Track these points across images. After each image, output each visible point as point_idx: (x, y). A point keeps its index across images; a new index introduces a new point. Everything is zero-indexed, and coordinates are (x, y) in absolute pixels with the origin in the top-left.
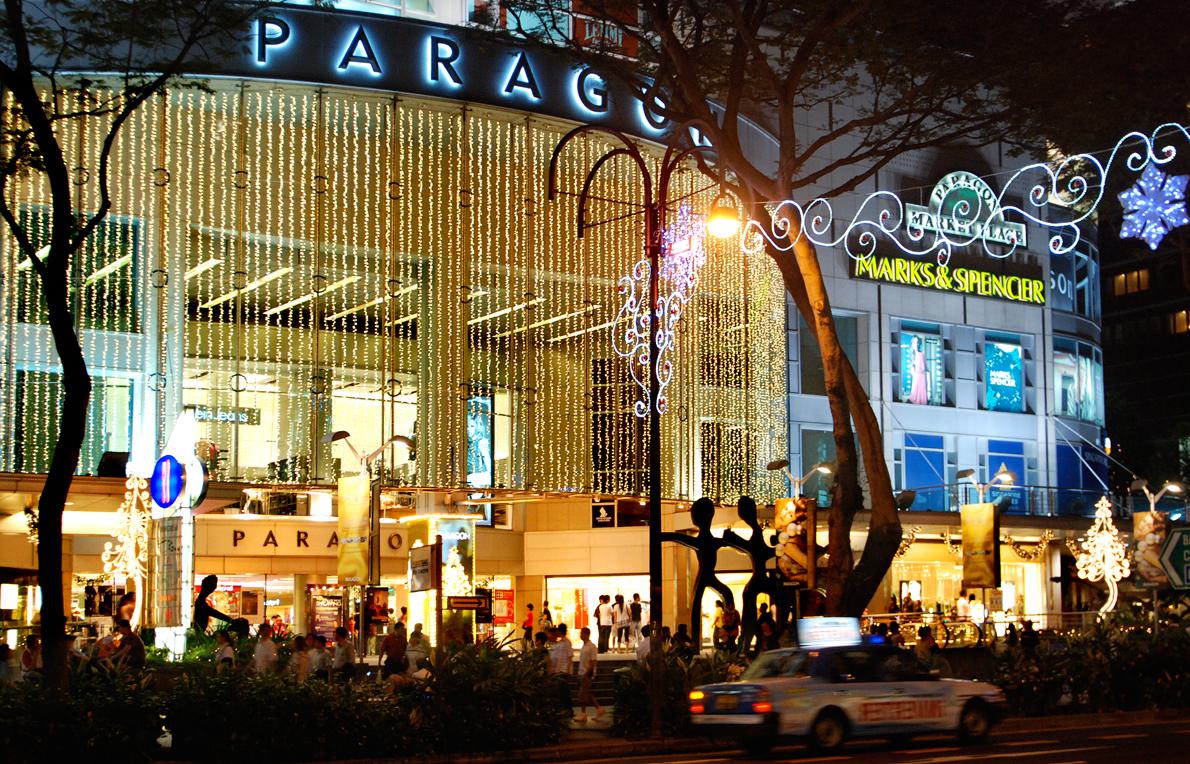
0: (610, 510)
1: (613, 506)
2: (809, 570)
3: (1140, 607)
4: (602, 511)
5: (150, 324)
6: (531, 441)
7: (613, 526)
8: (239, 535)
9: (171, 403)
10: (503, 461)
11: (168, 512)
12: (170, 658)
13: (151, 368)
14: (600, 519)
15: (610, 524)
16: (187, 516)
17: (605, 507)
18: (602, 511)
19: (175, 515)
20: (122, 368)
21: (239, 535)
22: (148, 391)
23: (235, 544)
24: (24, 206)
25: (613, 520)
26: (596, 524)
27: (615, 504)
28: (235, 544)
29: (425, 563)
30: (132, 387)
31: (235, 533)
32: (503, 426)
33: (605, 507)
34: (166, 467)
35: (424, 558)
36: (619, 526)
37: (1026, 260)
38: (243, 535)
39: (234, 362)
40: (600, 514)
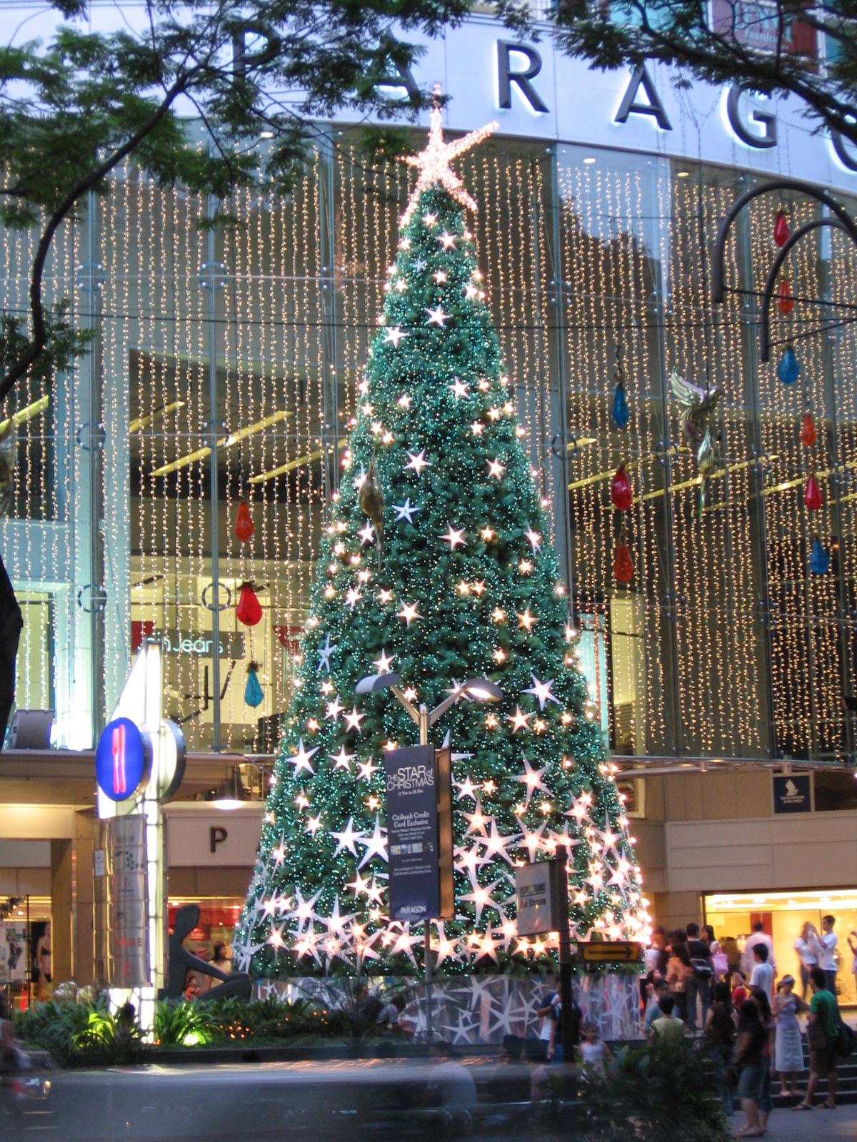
0: (801, 783)
1: (807, 778)
2: (172, 1045)
3: (693, 956)
4: (790, 786)
5: (79, 503)
6: (671, 681)
7: (808, 810)
8: (218, 835)
9: (116, 635)
10: (627, 708)
11: (124, 808)
12: (573, 981)
13: (83, 574)
14: (786, 800)
15: (804, 807)
16: (152, 811)
17: (794, 780)
18: (790, 786)
19: (135, 812)
20: (36, 577)
21: (218, 835)
22: (79, 612)
23: (213, 850)
24: (147, 503)
25: (807, 801)
26: (781, 808)
27: (811, 774)
28: (213, 850)
29: (540, 888)
30: (51, 606)
31: (213, 830)
32: (625, 650)
33: (794, 780)
34: (119, 736)
35: (539, 882)
36: (818, 808)
37: (787, 962)
38: (224, 833)
39: (209, 561)
40: (786, 791)
